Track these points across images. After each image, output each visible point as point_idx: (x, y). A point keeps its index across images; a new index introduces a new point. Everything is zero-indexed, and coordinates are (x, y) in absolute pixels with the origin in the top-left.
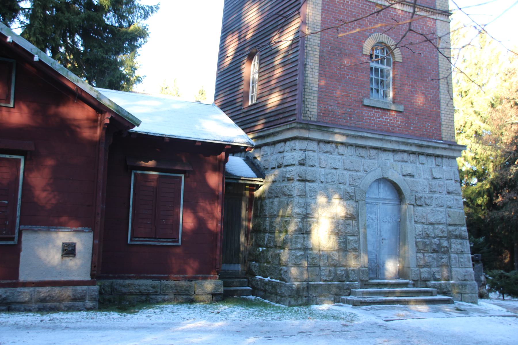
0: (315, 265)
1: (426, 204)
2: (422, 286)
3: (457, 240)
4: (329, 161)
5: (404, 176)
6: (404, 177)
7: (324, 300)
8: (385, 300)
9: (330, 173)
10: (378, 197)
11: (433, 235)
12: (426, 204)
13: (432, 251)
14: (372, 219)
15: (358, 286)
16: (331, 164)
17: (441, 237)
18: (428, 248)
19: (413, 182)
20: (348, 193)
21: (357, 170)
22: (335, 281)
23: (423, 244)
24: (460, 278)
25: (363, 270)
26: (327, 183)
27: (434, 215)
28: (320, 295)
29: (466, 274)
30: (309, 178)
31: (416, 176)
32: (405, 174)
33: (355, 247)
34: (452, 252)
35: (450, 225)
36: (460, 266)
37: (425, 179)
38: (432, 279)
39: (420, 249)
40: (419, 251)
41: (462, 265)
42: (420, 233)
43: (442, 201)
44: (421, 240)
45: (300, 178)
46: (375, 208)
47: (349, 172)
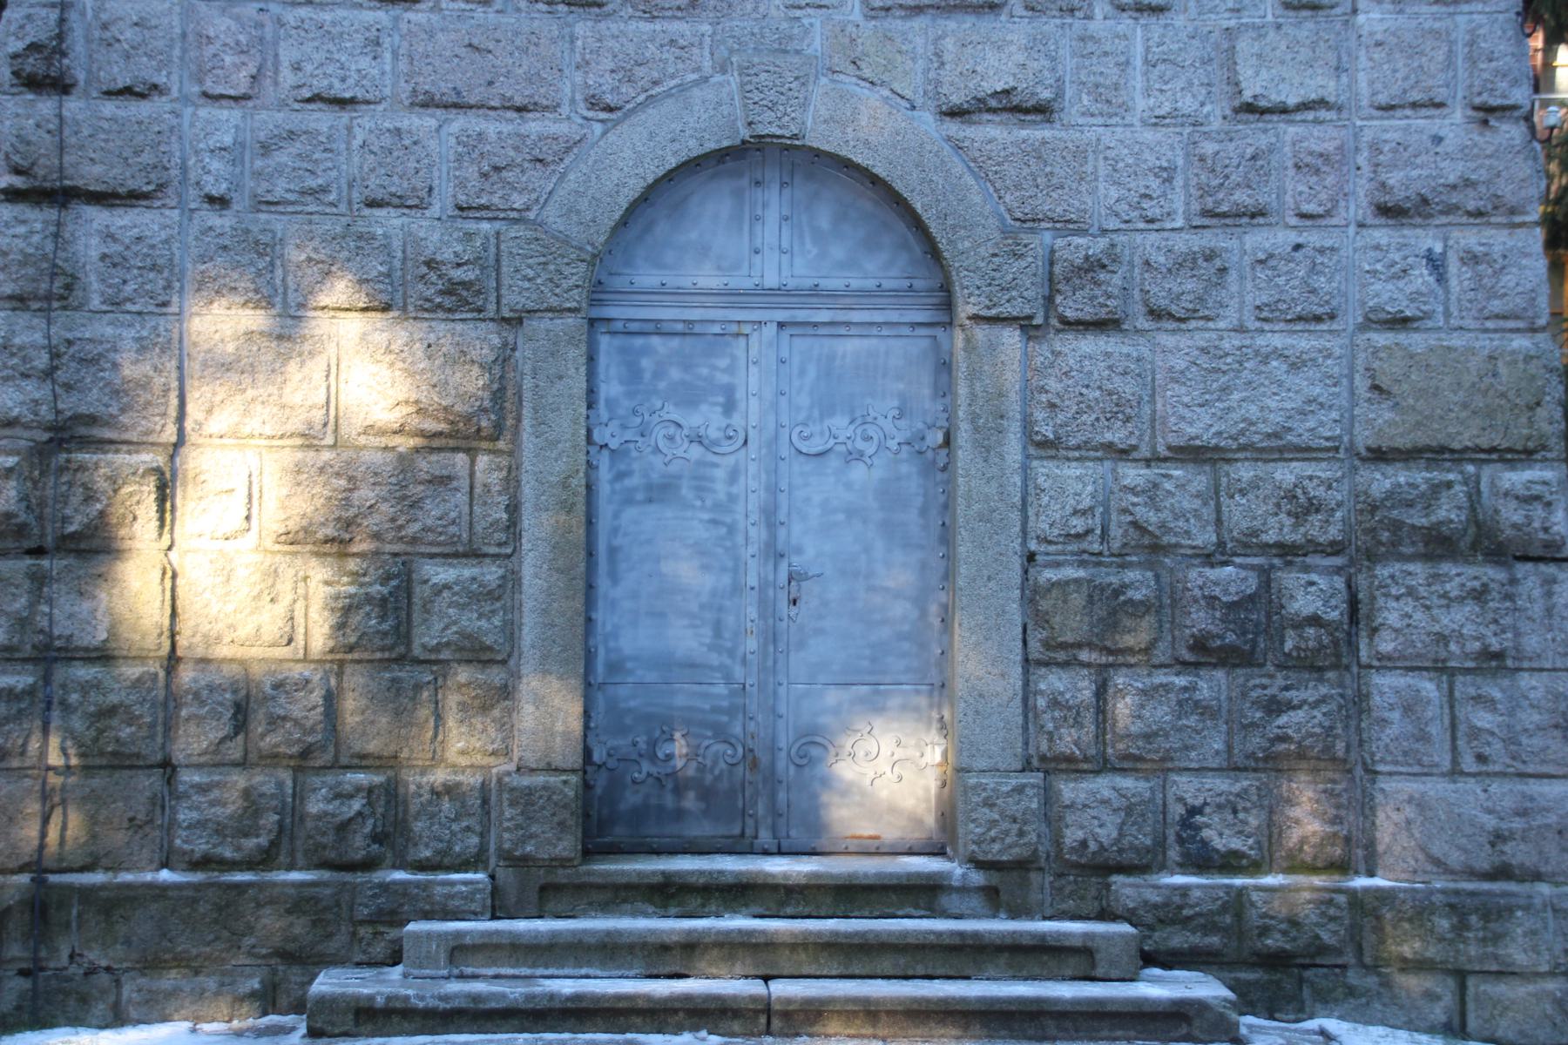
0: (122, 762)
1: (1155, 314)
2: (1070, 904)
3: (1447, 568)
4: (287, 54)
5: (955, 113)
6: (953, 127)
7: (173, 993)
8: (577, 997)
9: (292, 135)
10: (748, 284)
11: (1205, 537)
12: (1155, 314)
13: (1188, 656)
14: (698, 439)
15: (469, 897)
16: (297, 68)
17: (1287, 551)
18: (1136, 635)
19: (1037, 152)
22: (291, 867)
23: (1090, 600)
24: (1455, 859)
25: (529, 791)
26: (263, 204)
27: (1225, 390)
28: (151, 964)
29: (1517, 824)
30: (91, 174)
31: (1076, 105)
33: (463, 634)
34: (1386, 663)
35: (1379, 456)
36: (1469, 764)
37: (1158, 121)
38: (1174, 854)
39: (1069, 637)
40: (1061, 656)
41: (1481, 758)
42: (1078, 524)
43: (1320, 282)
44: (1081, 573)
45: (19, 182)
46: (723, 363)
47: (459, 123)
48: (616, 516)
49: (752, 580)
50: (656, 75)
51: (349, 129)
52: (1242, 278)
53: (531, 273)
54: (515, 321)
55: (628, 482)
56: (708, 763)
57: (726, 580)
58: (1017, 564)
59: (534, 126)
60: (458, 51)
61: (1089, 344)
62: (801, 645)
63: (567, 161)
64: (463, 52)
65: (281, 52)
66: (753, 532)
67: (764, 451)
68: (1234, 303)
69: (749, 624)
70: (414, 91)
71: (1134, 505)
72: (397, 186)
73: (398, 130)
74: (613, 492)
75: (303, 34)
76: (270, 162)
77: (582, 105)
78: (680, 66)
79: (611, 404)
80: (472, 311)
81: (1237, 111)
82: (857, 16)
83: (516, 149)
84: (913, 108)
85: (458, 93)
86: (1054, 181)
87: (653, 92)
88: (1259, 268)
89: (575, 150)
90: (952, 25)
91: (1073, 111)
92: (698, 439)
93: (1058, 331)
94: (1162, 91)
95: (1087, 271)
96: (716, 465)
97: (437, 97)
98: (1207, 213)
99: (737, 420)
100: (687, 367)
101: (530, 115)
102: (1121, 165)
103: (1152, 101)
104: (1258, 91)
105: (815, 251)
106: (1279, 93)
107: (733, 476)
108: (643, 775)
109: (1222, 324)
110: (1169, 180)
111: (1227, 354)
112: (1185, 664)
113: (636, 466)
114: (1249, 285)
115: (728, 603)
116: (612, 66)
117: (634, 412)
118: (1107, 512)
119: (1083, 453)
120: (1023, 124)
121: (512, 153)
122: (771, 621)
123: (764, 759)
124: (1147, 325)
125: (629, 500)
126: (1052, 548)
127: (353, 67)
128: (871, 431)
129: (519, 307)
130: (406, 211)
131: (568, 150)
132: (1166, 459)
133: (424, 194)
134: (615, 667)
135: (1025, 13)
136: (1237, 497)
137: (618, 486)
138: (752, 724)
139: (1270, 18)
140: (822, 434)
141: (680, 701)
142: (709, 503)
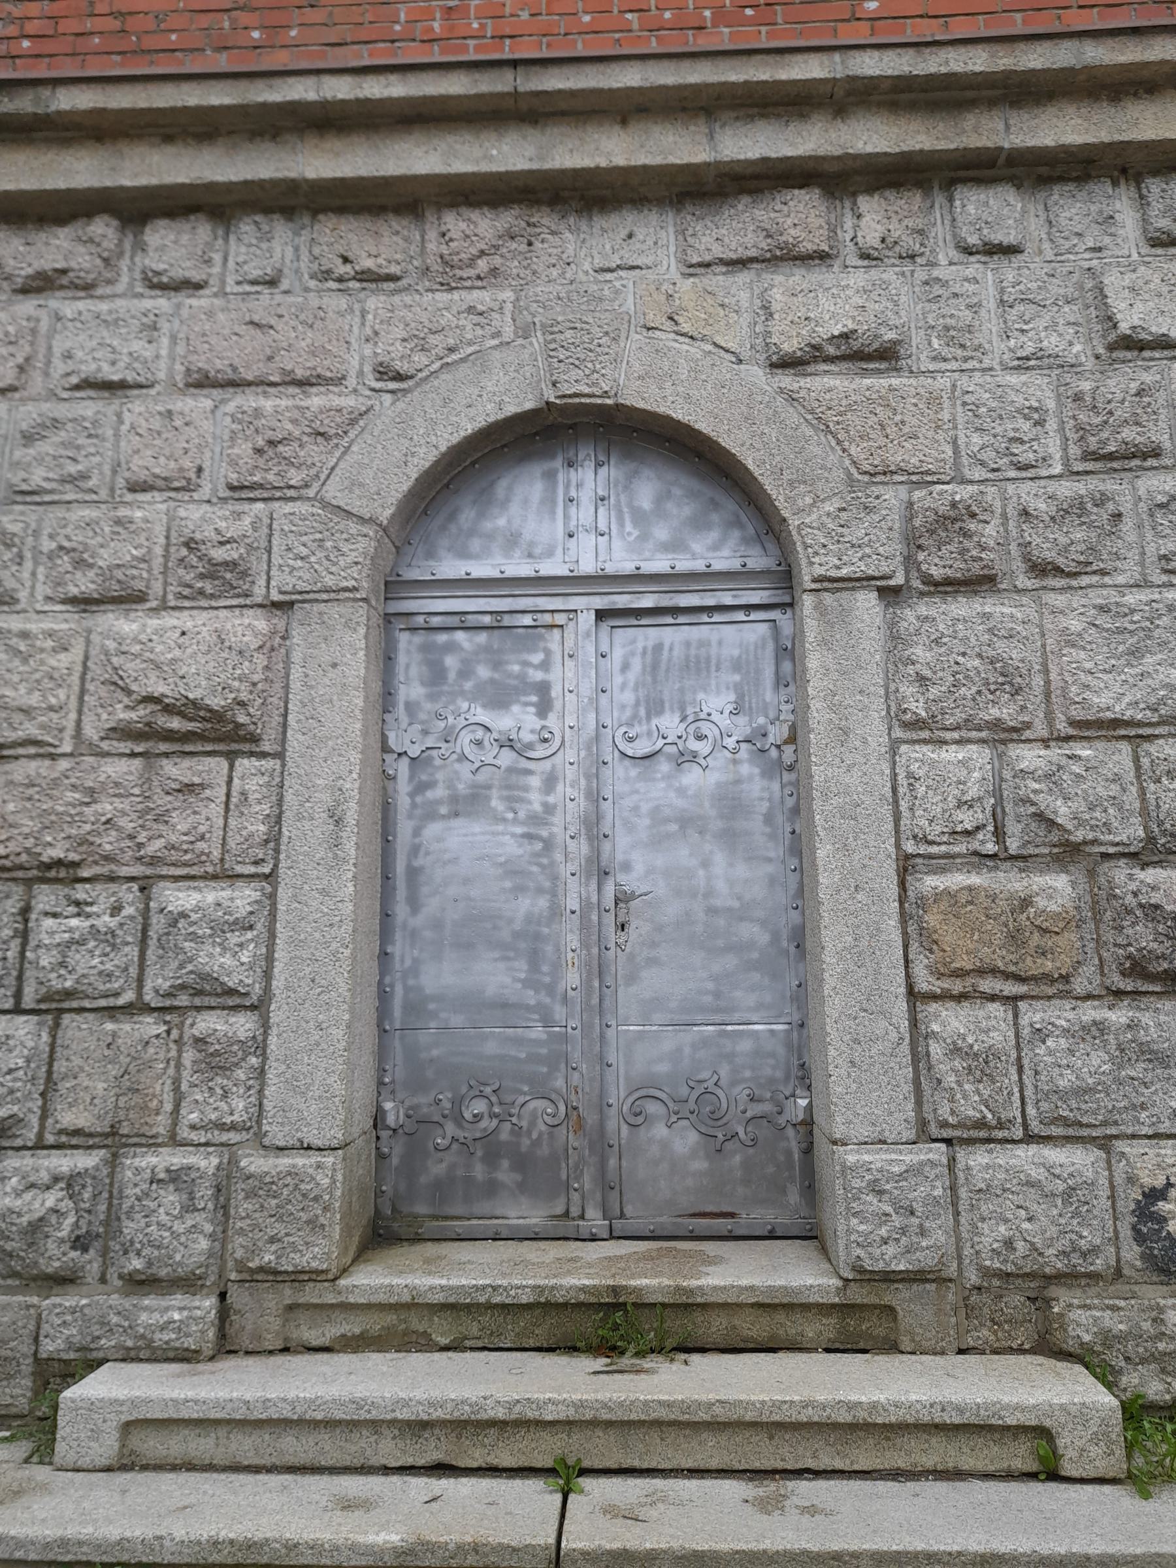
6: (786, 380)
11: (1132, 832)
12: (1040, 569)
20: (190, 544)
21: (300, 373)
32: (791, 346)
42: (966, 818)
46: (536, 658)
48: (417, 832)
49: (573, 903)
50: (451, 341)
51: (119, 415)
52: (1140, 526)
53: (304, 551)
54: (283, 606)
55: (430, 794)
56: (524, 1124)
57: (543, 903)
58: (890, 869)
59: (316, 400)
60: (237, 329)
61: (961, 607)
62: (632, 979)
63: (352, 434)
64: (242, 329)
65: (54, 343)
66: (572, 845)
67: (583, 754)
68: (1133, 555)
69: (570, 955)
70: (188, 370)
71: (1035, 792)
72: (163, 467)
73: (170, 412)
74: (414, 805)
75: (79, 325)
76: (31, 451)
77: (371, 376)
78: (479, 332)
79: (411, 708)
80: (238, 596)
81: (1111, 348)
82: (674, 273)
83: (294, 422)
84: (740, 361)
85: (235, 369)
86: (906, 429)
87: (449, 360)
88: (1159, 514)
89: (361, 423)
90: (779, 278)
91: (923, 357)
92: (508, 743)
93: (922, 594)
94: (1023, 331)
95: (954, 520)
96: (529, 772)
97: (212, 373)
98: (1090, 456)
99: (552, 721)
100: (497, 665)
101: (314, 390)
102: (983, 410)
103: (1012, 342)
104: (1137, 322)
105: (636, 533)
106: (1159, 325)
107: (550, 782)
108: (446, 1142)
109: (1121, 579)
110: (1040, 423)
111: (1133, 611)
112: (1119, 994)
113: (440, 776)
114: (1149, 535)
115: (546, 930)
116: (404, 334)
117: (439, 716)
118: (1000, 800)
119: (964, 733)
120: (865, 373)
121: (289, 426)
122: (595, 951)
123: (591, 1119)
124: (1029, 584)
125: (431, 815)
126: (934, 849)
127: (125, 351)
128: (705, 728)
129: (289, 588)
130: (172, 494)
131: (353, 422)
132: (1068, 738)
133: (192, 475)
134: (416, 1007)
135: (860, 263)
136: (1164, 780)
137: (419, 799)
138: (576, 1075)
139: (1135, 256)
140: (649, 734)
141: (491, 1048)
142: (522, 815)
